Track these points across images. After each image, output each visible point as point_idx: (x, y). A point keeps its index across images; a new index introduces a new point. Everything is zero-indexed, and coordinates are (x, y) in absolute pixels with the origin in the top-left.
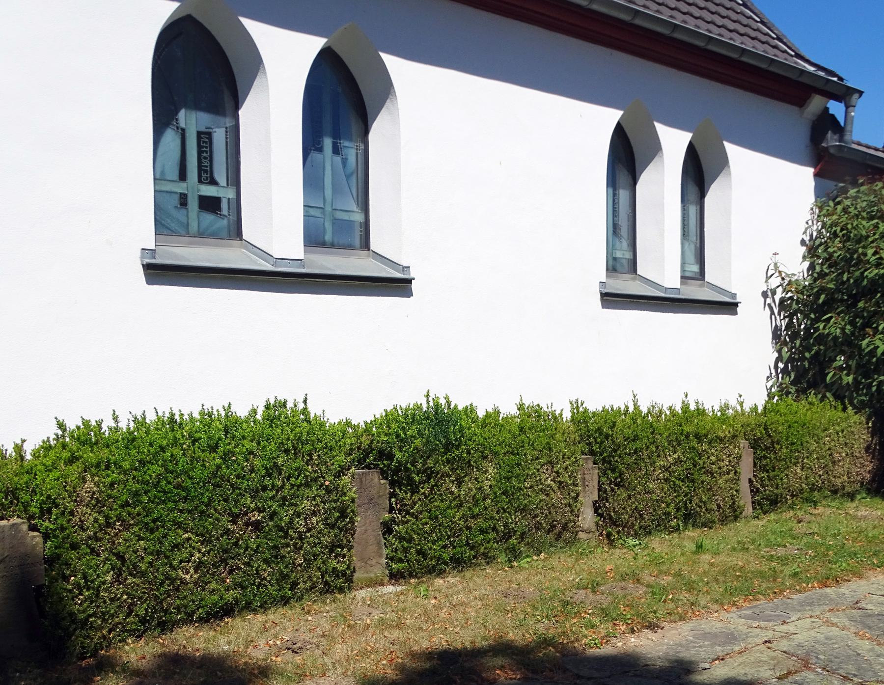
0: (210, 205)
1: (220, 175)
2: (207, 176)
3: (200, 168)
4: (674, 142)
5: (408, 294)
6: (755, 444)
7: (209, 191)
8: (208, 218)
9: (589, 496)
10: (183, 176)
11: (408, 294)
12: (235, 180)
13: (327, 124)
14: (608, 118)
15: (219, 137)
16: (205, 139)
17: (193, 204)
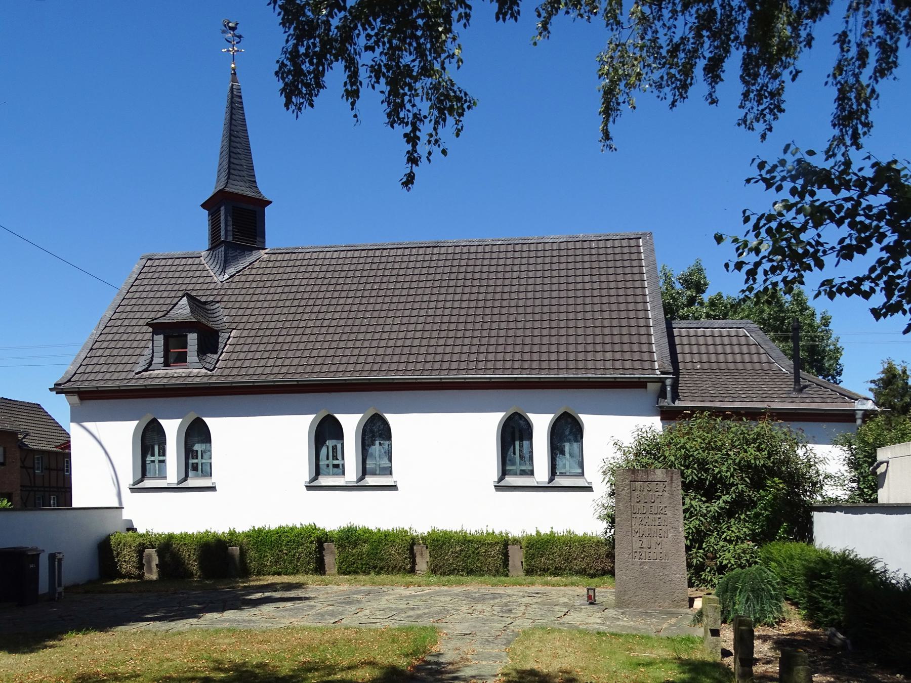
0: (336, 466)
1: (339, 457)
2: (335, 457)
3: (333, 456)
4: (541, 424)
5: (397, 490)
6: (160, 553)
7: (336, 462)
8: (336, 470)
9: (335, 588)
10: (328, 459)
11: (397, 490)
12: (343, 458)
13: (517, 435)
14: (492, 421)
15: (339, 446)
16: (335, 448)
17: (331, 466)
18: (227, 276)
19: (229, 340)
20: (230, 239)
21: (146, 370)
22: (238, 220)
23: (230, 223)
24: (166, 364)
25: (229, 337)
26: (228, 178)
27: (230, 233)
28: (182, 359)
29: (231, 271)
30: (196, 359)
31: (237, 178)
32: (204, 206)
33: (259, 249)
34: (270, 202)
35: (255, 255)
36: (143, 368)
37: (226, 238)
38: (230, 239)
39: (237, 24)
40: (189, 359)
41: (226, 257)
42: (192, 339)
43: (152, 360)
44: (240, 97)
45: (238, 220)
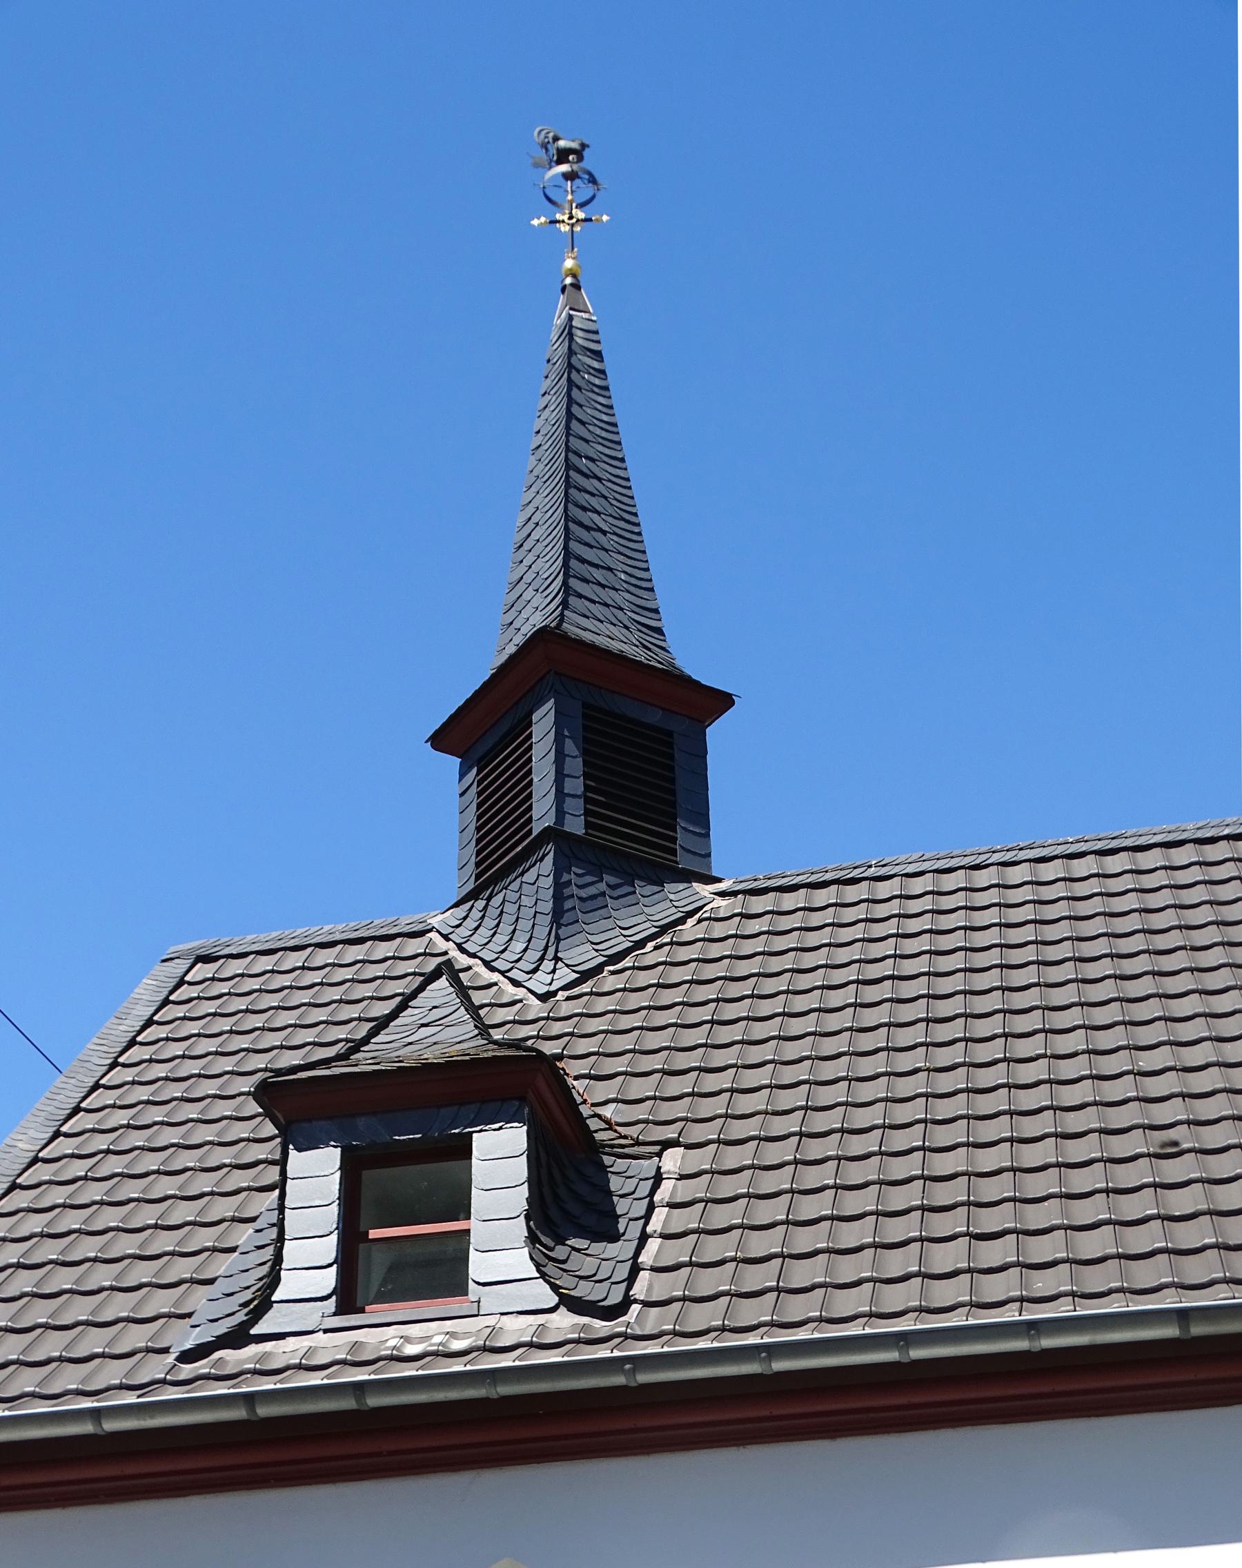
18: (565, 975)
19: (662, 1189)
20: (576, 826)
21: (238, 1338)
22: (596, 755)
23: (575, 765)
24: (348, 1298)
25: (658, 1178)
26: (565, 604)
27: (575, 807)
28: (440, 1272)
29: (582, 954)
30: (519, 1262)
31: (596, 609)
32: (440, 740)
33: (689, 877)
34: (721, 701)
35: (679, 895)
36: (222, 1328)
37: (560, 814)
38: (576, 826)
39: (584, 146)
40: (479, 1266)
41: (558, 898)
42: (499, 1158)
43: (273, 1280)
44: (598, 355)
45: (596, 755)
